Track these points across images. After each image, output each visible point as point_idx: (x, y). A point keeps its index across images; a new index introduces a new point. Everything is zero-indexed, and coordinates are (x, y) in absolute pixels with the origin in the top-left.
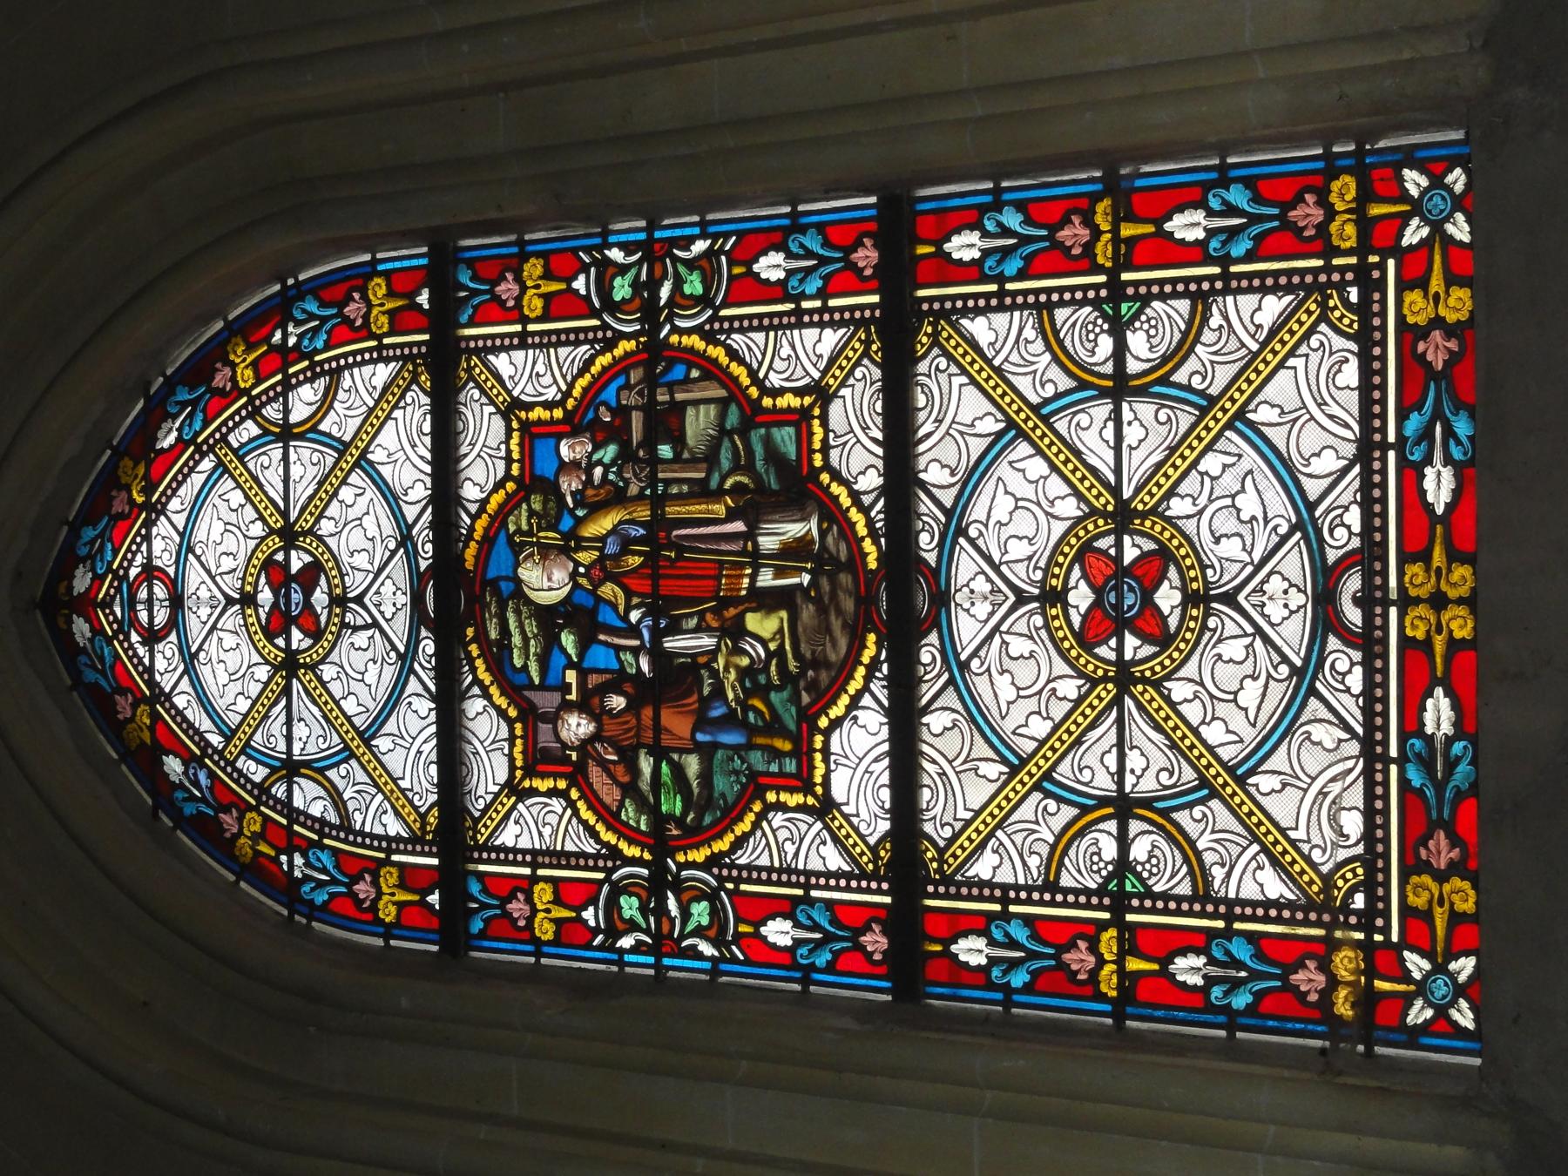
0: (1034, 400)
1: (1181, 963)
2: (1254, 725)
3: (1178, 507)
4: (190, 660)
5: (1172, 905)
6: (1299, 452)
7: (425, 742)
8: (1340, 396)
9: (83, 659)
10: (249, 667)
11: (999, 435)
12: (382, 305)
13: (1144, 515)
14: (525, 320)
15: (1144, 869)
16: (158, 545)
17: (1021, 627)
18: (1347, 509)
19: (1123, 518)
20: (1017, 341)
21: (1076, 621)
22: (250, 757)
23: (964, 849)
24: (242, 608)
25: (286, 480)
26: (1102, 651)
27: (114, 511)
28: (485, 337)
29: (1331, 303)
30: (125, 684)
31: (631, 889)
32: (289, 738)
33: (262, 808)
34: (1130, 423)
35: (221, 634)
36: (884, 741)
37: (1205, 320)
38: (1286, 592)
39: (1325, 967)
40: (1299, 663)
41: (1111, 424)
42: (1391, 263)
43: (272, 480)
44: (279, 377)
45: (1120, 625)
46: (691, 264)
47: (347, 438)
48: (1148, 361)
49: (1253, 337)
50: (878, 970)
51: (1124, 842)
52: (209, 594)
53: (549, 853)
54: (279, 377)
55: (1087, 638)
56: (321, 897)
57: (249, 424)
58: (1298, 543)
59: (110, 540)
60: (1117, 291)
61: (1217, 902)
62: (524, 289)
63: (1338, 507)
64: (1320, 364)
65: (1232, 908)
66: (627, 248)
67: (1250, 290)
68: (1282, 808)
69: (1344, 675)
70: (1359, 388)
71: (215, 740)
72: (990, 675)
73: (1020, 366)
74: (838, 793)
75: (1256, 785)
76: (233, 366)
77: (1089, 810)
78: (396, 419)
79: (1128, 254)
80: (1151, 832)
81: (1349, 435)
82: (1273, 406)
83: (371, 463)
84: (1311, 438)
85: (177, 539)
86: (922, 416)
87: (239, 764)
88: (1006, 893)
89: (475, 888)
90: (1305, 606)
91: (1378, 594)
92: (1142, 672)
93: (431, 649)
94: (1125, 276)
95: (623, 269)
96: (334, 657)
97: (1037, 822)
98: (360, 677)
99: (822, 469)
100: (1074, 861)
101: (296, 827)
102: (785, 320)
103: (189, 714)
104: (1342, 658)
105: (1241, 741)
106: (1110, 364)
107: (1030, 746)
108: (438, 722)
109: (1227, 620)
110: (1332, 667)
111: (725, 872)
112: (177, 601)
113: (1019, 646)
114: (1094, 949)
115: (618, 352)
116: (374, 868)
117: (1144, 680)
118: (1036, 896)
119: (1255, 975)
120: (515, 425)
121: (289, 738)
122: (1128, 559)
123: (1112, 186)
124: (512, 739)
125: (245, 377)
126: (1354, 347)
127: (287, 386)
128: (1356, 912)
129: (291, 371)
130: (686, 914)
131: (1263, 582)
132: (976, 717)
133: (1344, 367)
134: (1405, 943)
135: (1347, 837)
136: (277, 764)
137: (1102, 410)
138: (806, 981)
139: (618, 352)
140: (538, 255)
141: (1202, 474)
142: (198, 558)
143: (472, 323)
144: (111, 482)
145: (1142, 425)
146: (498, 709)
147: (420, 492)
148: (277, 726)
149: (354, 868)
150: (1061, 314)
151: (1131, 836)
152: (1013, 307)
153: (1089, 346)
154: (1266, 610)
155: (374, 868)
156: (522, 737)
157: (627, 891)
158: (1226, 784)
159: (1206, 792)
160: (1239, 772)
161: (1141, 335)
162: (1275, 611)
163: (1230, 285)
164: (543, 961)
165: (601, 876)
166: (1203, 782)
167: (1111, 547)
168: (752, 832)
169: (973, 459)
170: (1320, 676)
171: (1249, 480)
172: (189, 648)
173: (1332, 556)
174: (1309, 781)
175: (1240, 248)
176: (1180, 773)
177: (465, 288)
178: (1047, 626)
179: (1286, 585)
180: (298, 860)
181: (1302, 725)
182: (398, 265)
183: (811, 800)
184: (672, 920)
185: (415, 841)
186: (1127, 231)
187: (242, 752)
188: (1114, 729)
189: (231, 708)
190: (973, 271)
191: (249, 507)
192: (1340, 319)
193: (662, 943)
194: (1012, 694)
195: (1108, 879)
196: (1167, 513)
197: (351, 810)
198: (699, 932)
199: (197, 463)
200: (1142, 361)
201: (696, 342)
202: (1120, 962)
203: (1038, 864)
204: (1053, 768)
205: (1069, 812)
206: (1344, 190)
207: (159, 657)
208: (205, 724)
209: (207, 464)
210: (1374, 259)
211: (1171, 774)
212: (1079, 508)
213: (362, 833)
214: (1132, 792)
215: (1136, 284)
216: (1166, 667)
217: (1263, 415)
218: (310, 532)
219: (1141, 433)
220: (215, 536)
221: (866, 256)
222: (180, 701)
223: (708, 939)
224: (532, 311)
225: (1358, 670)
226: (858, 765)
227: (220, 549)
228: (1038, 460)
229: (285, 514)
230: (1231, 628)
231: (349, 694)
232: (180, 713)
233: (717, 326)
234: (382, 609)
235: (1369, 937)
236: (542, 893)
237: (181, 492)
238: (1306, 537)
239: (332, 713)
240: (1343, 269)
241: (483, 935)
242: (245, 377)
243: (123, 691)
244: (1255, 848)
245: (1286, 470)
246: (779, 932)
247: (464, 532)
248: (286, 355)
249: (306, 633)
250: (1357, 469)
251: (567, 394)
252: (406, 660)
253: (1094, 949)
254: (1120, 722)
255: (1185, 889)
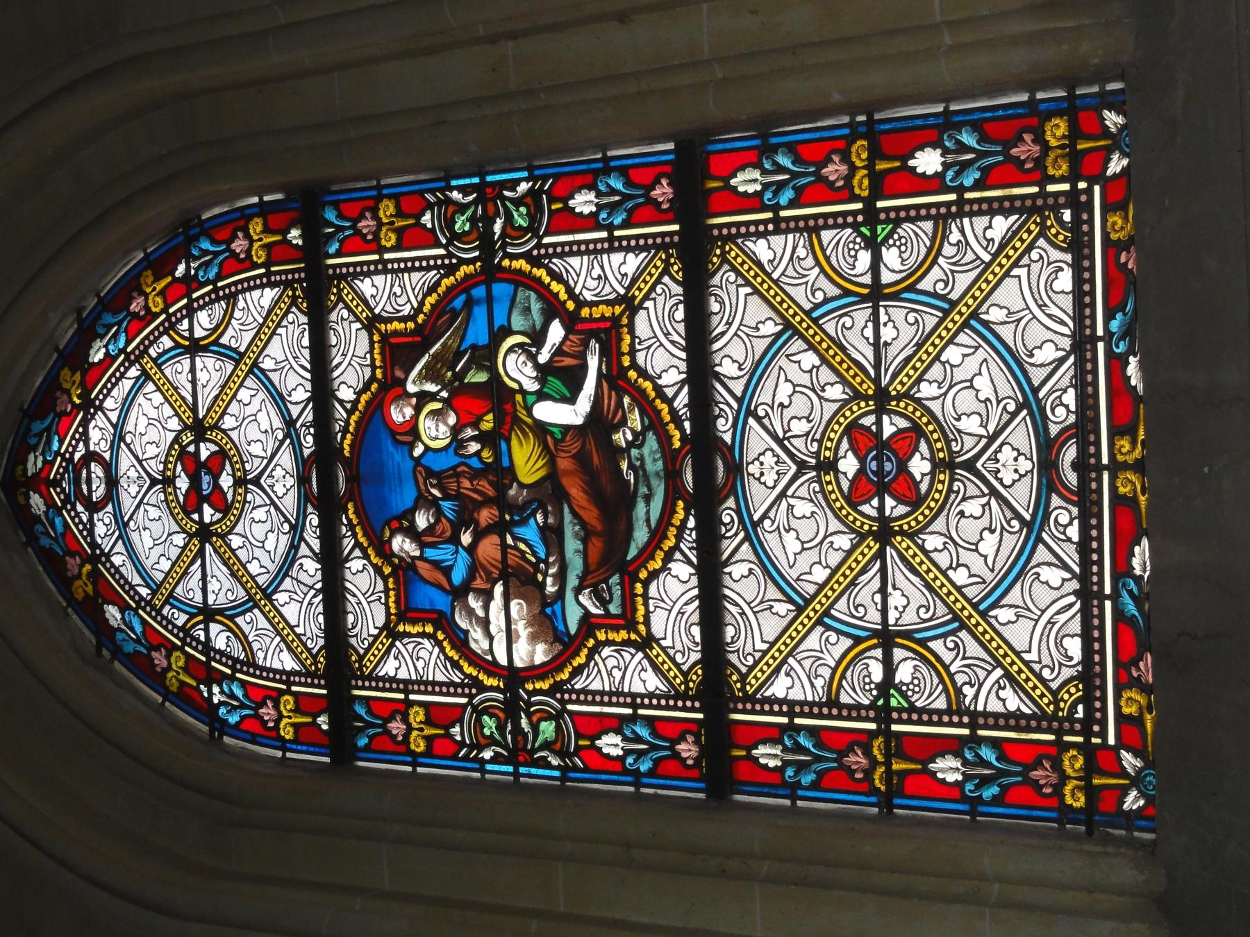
0: (963, 634)
1: (761, 750)
2: (992, 571)
3: (926, 390)
4: (122, 525)
5: (935, 718)
6: (1024, 345)
7: (686, 604)
8: (1060, 299)
9: (39, 528)
10: (169, 535)
11: (778, 335)
12: (260, 240)
13: (899, 397)
14: (381, 250)
15: (908, 689)
16: (94, 435)
17: (803, 492)
18: (1065, 391)
19: (882, 401)
20: (791, 259)
21: (845, 485)
22: (174, 607)
23: (763, 672)
24: (164, 488)
25: (194, 382)
26: (866, 509)
27: (58, 409)
28: (347, 265)
29: (1049, 223)
30: (74, 548)
31: (491, 710)
32: (204, 591)
33: (187, 649)
34: (885, 324)
35: (147, 507)
36: (694, 588)
37: (945, 237)
38: (284, 477)
39: (405, 720)
40: (1028, 517)
41: (870, 325)
42: (1097, 189)
43: (183, 381)
44: (185, 301)
45: (881, 489)
46: (518, 202)
47: (242, 349)
48: (901, 272)
49: (985, 249)
50: (689, 774)
51: (889, 668)
52: (137, 475)
53: (419, 682)
54: (185, 301)
55: (854, 499)
56: (233, 719)
57: (165, 339)
58: (1024, 418)
59: (57, 433)
60: (871, 216)
61: (967, 712)
62: (251, 241)
63: (1061, 389)
64: (1039, 276)
65: (976, 719)
66: (464, 190)
67: (980, 213)
68: (1018, 635)
69: (1066, 526)
70: (1073, 291)
71: (144, 592)
72: (997, 397)
73: (795, 278)
74: (657, 630)
75: (776, 324)
76: (146, 296)
77: (908, 288)
78: (280, 335)
79: (880, 186)
80: (915, 659)
81: (1066, 331)
82: (1001, 308)
83: (263, 371)
84: (1035, 334)
85: (112, 431)
86: (334, 350)
87: (165, 612)
88: (791, 707)
89: (360, 710)
90: (1032, 471)
91: (1093, 461)
92: (901, 526)
93: (315, 522)
94: (880, 204)
95: (462, 208)
96: (239, 529)
97: (953, 272)
98: (261, 545)
99: (629, 368)
100: (850, 681)
101: (213, 664)
102: (599, 246)
103: (123, 570)
104: (1063, 515)
105: (984, 582)
106: (869, 275)
107: (811, 589)
108: (700, 586)
109: (968, 483)
110: (1056, 520)
111: (566, 696)
112: (112, 482)
113: (803, 508)
114: (868, 753)
115: (460, 274)
116: (276, 696)
117: (902, 533)
118: (825, 711)
119: (654, 747)
120: (376, 338)
121: (204, 591)
122: (886, 435)
123: (870, 132)
124: (386, 591)
125: (156, 304)
126: (1068, 257)
127: (190, 312)
128: (1078, 720)
129: (195, 295)
130: (535, 728)
131: (996, 452)
132: (767, 566)
133: (1060, 274)
134: (1122, 743)
135: (1071, 659)
136: (863, 634)
137: (862, 315)
138: (973, 813)
139: (460, 274)
140: (390, 197)
141: (943, 363)
142: (128, 446)
143: (338, 254)
144: (52, 387)
145: (895, 327)
146: (375, 566)
147: (301, 395)
148: (194, 581)
149: (258, 697)
150: (826, 235)
151: (896, 662)
152: (787, 231)
153: (851, 261)
154: (275, 489)
155: (276, 696)
156: (637, 595)
157: (486, 711)
158: (971, 616)
159: (956, 624)
160: (790, 332)
161: (894, 251)
162: (280, 490)
163: (962, 210)
164: (419, 770)
165: (464, 700)
166: (251, 599)
167: (873, 424)
168: (587, 664)
169: (1018, 585)
170: (1047, 529)
171: (985, 364)
172: (122, 518)
173: (1054, 430)
174: (1039, 613)
175: (787, 196)
176: (935, 609)
177: (331, 224)
178: (822, 491)
179: (1015, 453)
180: (216, 689)
181: (1032, 568)
182: (630, 162)
183: (383, 327)
184: (525, 735)
185: (309, 675)
186: (882, 166)
187: (166, 602)
188: (878, 577)
189: (155, 567)
190: (753, 202)
191: (166, 406)
192: (1056, 236)
193: (519, 753)
194: (977, 382)
195: (877, 698)
196: (917, 395)
197: (255, 650)
198: (547, 745)
199: (127, 369)
200: (893, 271)
201: (521, 264)
202: (888, 764)
203: (822, 684)
204: (831, 606)
205: (925, 285)
206: (1057, 130)
207: (99, 525)
208: (136, 580)
209: (134, 372)
210: (1082, 185)
211: (843, 325)
212: (844, 392)
213: (263, 669)
214: (895, 625)
215: (887, 210)
216: (920, 522)
217: (995, 315)
218: (216, 427)
219: (894, 334)
220: (141, 429)
221: (663, 192)
222: (117, 560)
223: (553, 751)
224: (259, 258)
225: (1076, 522)
226: (1040, 617)
227: (145, 439)
228: (158, 394)
229: (194, 409)
230: (972, 490)
231: (253, 558)
232: (117, 570)
233: (543, 251)
234: (999, 476)
235: (1088, 740)
236: (417, 716)
237: (115, 393)
238: (1031, 413)
239: (237, 571)
240: (1056, 195)
241: (367, 748)
242: (156, 304)
243: (72, 554)
244: (278, 639)
245: (1015, 362)
246: (611, 744)
247: (342, 424)
248: (190, 282)
249: (217, 510)
250: (1072, 359)
251: (419, 310)
252: (296, 529)
253: (868, 753)
254: (883, 571)
255: (941, 704)
